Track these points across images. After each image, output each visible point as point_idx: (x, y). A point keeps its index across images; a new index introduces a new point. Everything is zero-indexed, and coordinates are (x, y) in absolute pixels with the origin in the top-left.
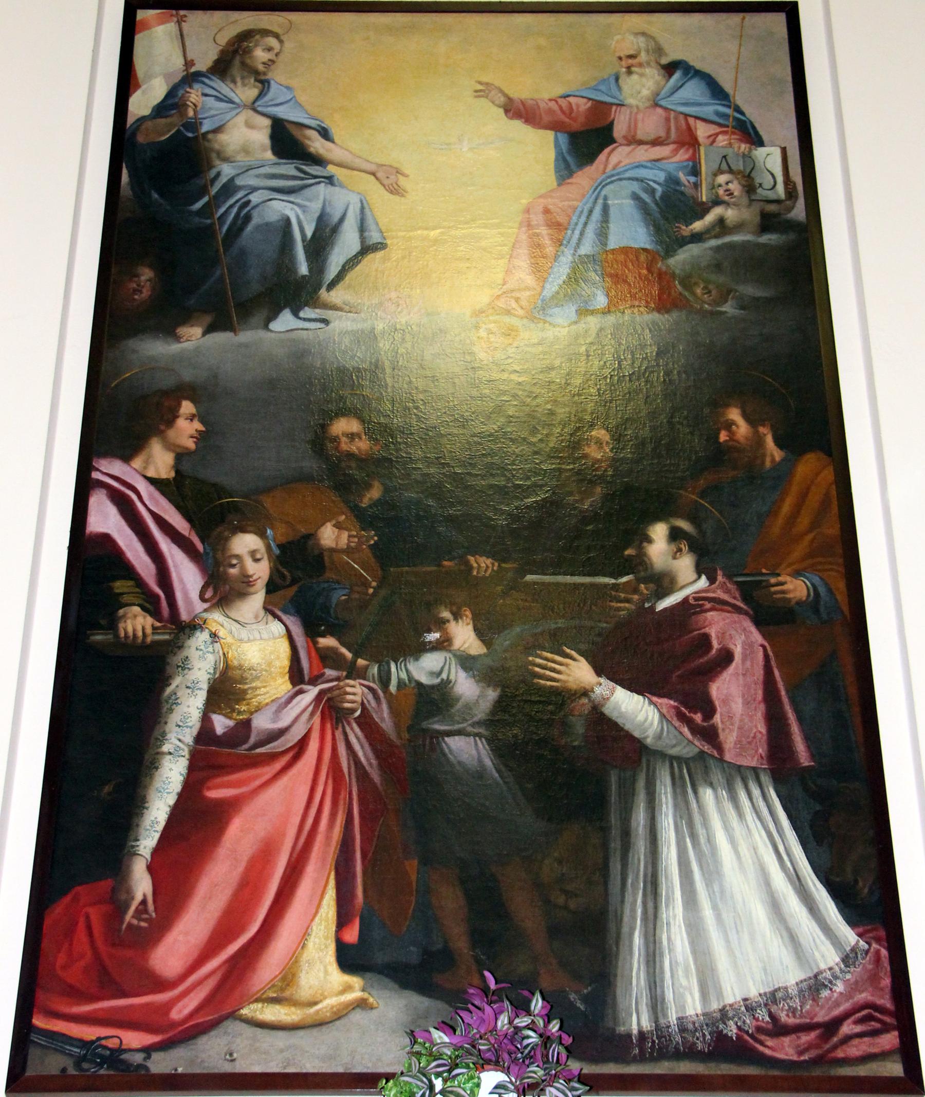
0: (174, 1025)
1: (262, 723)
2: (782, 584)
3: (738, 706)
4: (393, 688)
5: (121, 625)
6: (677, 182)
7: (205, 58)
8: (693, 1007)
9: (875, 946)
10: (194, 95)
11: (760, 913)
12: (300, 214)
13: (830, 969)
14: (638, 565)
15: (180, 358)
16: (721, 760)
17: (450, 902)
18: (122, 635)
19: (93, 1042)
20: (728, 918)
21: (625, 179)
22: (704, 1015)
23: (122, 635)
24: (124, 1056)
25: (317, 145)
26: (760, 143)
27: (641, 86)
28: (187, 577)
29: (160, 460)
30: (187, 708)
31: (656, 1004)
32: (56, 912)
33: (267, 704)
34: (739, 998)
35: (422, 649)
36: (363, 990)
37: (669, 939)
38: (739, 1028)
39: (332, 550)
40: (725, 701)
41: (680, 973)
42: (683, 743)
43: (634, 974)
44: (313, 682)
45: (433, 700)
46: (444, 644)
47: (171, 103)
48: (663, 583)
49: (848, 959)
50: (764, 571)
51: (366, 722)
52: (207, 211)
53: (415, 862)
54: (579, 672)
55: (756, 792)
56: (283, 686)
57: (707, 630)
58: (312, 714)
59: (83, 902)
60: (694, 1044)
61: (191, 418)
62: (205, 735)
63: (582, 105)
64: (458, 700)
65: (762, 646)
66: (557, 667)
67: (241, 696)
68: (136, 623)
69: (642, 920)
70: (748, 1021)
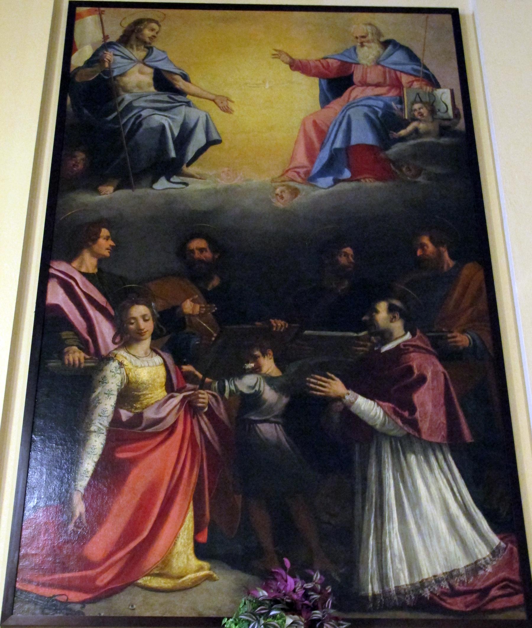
0: (98, 588)
1: (150, 414)
3: (429, 407)
4: (227, 395)
5: (66, 357)
6: (391, 107)
7: (115, 33)
8: (405, 580)
9: (510, 545)
10: (109, 55)
11: (443, 526)
12: (171, 123)
16: (420, 439)
20: (424, 529)
23: (67, 362)
25: (181, 84)
26: (437, 85)
28: (105, 330)
29: (89, 263)
30: (106, 405)
31: (383, 579)
33: (152, 404)
34: (431, 575)
35: (242, 373)
37: (390, 541)
38: (431, 592)
41: (397, 561)
42: (397, 428)
43: (370, 561)
44: (180, 391)
45: (251, 401)
46: (257, 370)
47: (96, 59)
48: (385, 336)
49: (494, 553)
51: (211, 414)
52: (116, 120)
54: (336, 387)
55: (440, 457)
56: (161, 393)
57: (411, 363)
58: (179, 410)
62: (116, 420)
63: (334, 63)
67: (137, 399)
68: (75, 356)
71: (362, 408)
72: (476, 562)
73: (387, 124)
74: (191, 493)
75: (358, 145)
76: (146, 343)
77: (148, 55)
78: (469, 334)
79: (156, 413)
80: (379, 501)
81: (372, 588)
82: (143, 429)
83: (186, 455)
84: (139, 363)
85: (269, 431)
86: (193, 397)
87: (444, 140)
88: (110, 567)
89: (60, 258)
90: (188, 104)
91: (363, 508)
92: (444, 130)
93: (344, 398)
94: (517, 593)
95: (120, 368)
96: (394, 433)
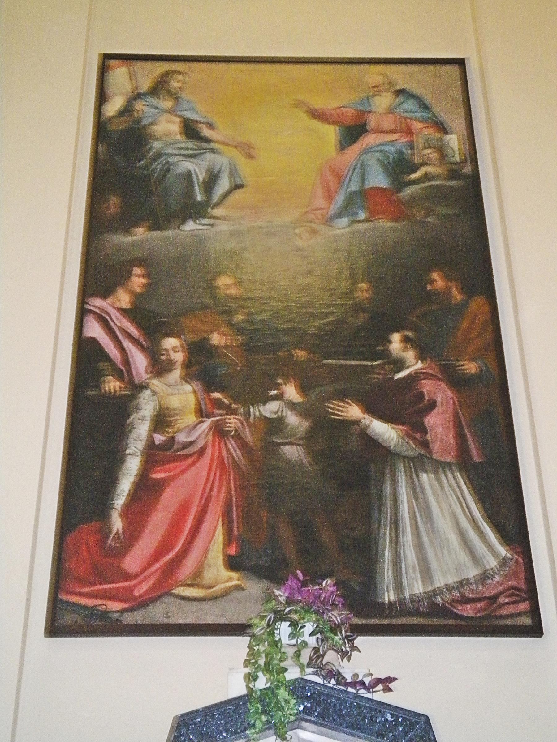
0: (136, 598)
1: (182, 438)
2: (463, 365)
3: (440, 430)
4: (252, 420)
5: (102, 386)
6: (402, 153)
7: (145, 85)
9: (516, 556)
10: (139, 105)
11: (454, 539)
12: (198, 169)
13: (492, 569)
14: (385, 354)
15: (134, 245)
16: (431, 458)
17: (286, 533)
18: (103, 391)
19: (92, 607)
21: (378, 151)
22: (424, 593)
23: (103, 391)
24: (110, 615)
25: (206, 132)
26: (446, 133)
27: (383, 102)
28: (140, 361)
29: (123, 299)
30: (141, 431)
31: (399, 587)
32: (71, 538)
33: (183, 429)
34: (443, 584)
35: (266, 400)
36: (238, 580)
37: (404, 553)
38: (443, 600)
39: (217, 347)
40: (432, 428)
42: (411, 449)
43: (386, 572)
44: (208, 416)
45: (275, 425)
46: (279, 397)
47: (126, 111)
48: (399, 364)
50: (452, 358)
51: (238, 437)
52: (146, 167)
53: (266, 512)
54: (354, 411)
55: (450, 475)
56: (192, 419)
57: (422, 390)
58: (208, 433)
59: (85, 533)
60: (419, 608)
61: (139, 276)
62: (151, 445)
63: (350, 112)
64: (287, 426)
65: (453, 399)
66: (341, 409)
67: (169, 424)
68: (112, 385)
69: (389, 543)
70: (448, 596)
71: (377, 431)
72: (484, 573)
73: (400, 168)
74: (219, 511)
75: (373, 189)
76: (176, 374)
77: (176, 106)
78: (476, 362)
79: (187, 437)
80: (393, 515)
81: (389, 598)
82: (174, 452)
83: (215, 475)
84: (170, 390)
85: (292, 452)
86: (220, 422)
87: (454, 183)
88: (145, 579)
89: (95, 295)
90: (213, 151)
91: (379, 523)
92: (454, 174)
93: (360, 421)
94: (524, 601)
95: (153, 395)
96: (409, 453)
